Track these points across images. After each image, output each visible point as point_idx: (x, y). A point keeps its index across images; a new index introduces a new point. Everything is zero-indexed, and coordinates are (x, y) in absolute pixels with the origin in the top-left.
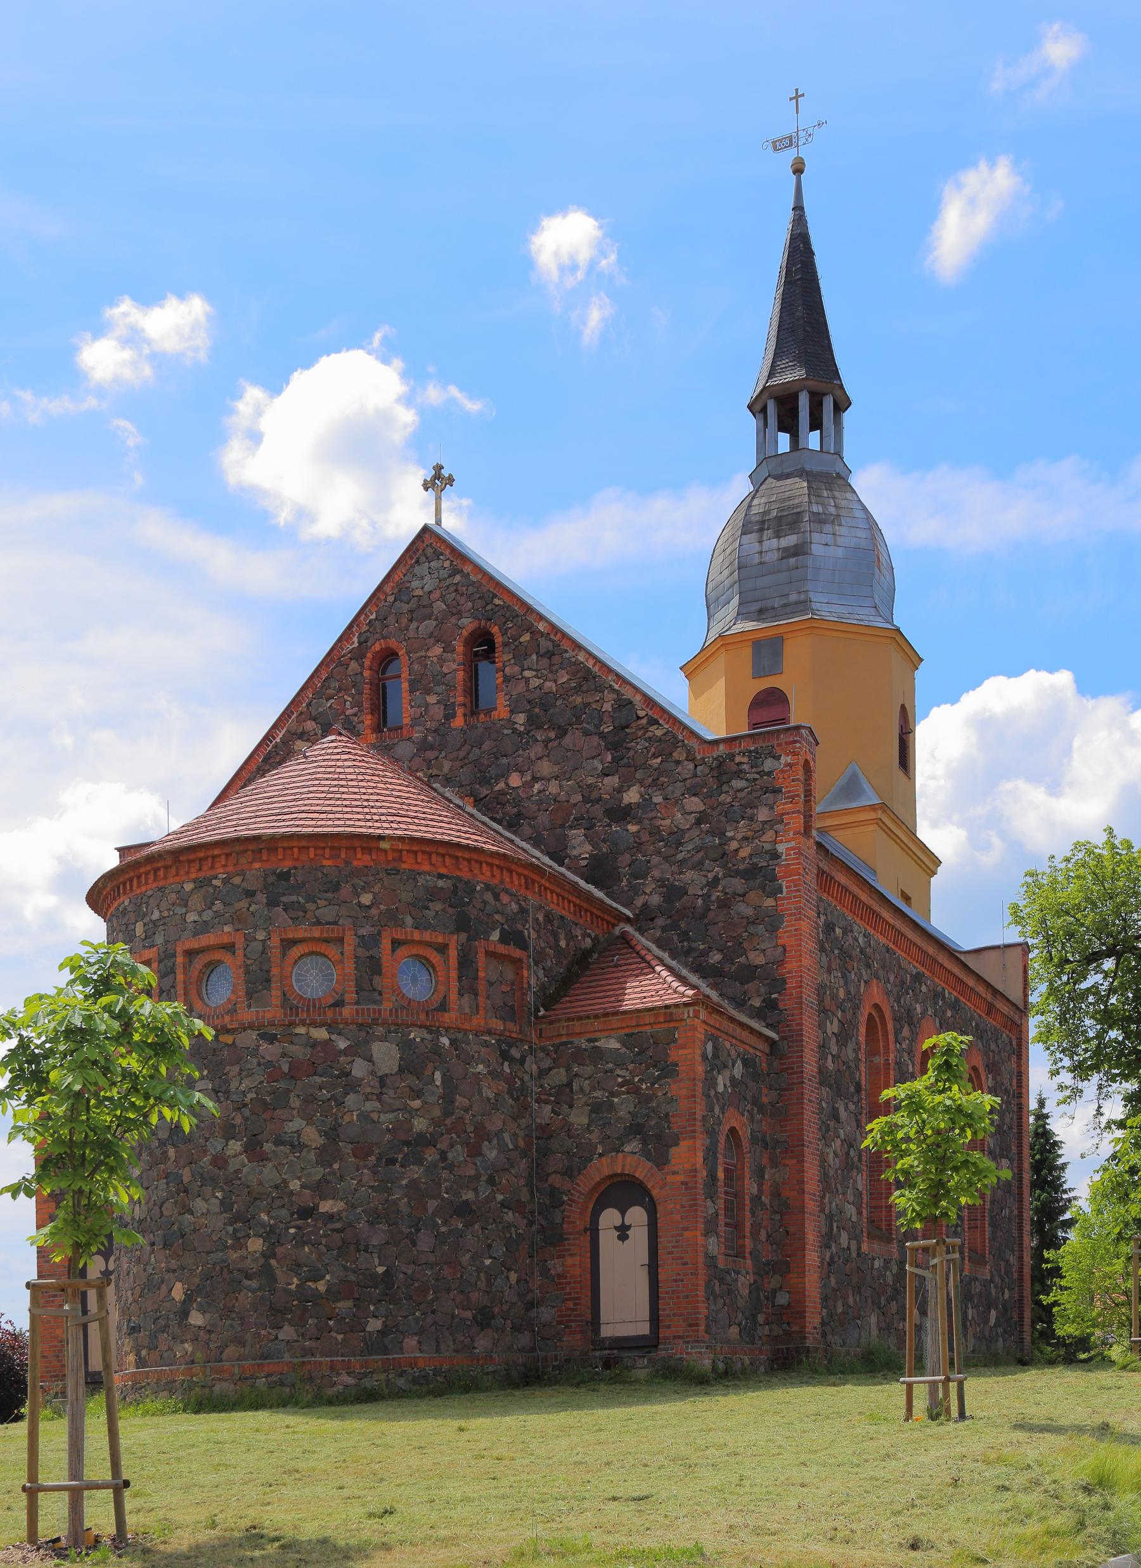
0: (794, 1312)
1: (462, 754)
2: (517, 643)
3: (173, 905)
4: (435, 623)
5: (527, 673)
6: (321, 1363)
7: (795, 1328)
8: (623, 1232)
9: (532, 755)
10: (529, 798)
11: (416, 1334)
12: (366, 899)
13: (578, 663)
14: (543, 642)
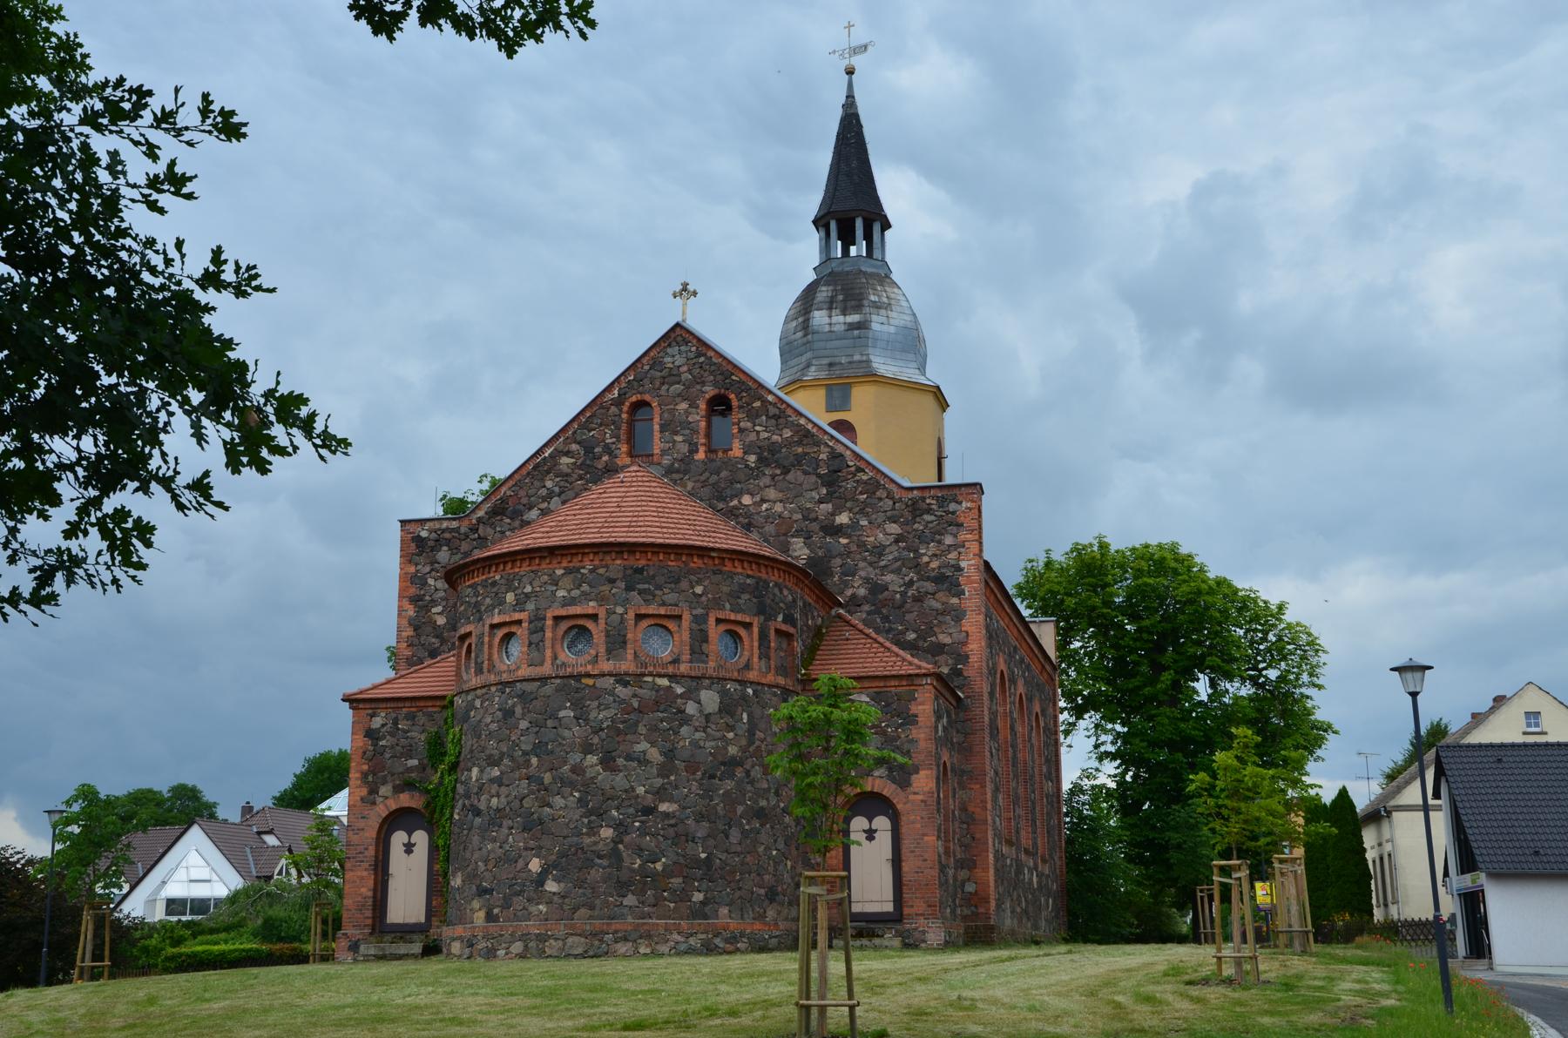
7: (982, 910)
8: (870, 834)
12: (699, 590)
14: (771, 408)
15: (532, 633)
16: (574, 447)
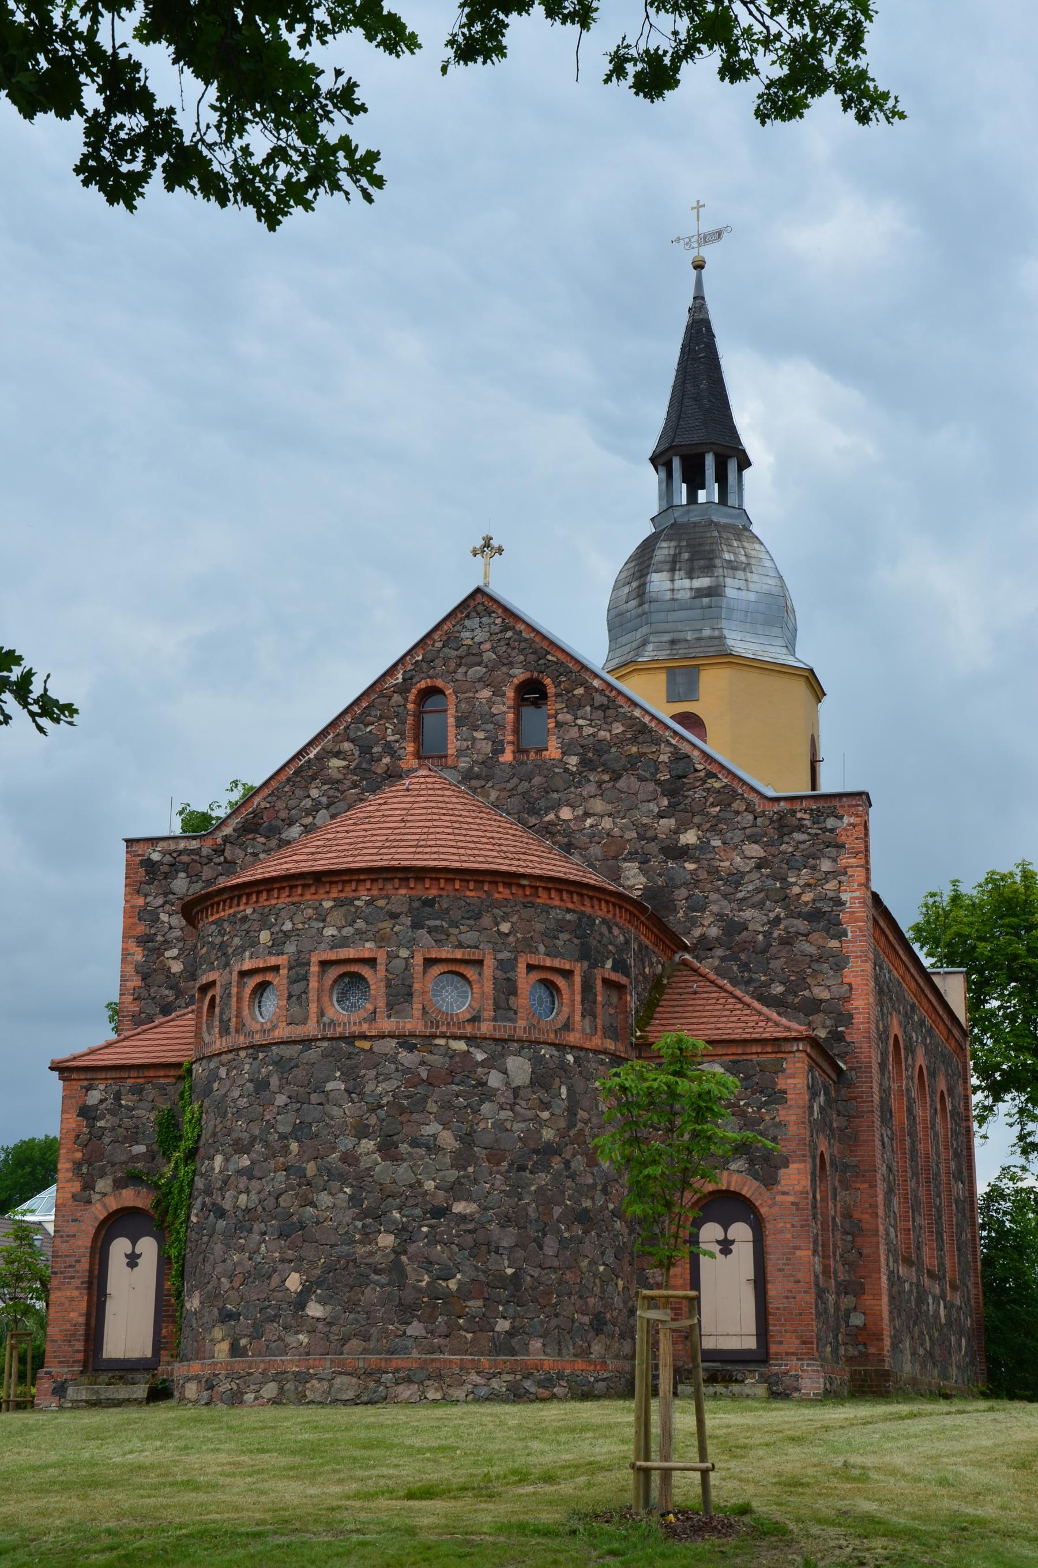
0: (866, 1335)
1: (509, 786)
2: (570, 695)
3: (310, 919)
4: (484, 670)
5: (580, 722)
6: (451, 1361)
9: (585, 793)
10: (581, 831)
11: (540, 1336)
12: (505, 927)
13: (633, 718)
15: (292, 982)
16: (347, 746)
